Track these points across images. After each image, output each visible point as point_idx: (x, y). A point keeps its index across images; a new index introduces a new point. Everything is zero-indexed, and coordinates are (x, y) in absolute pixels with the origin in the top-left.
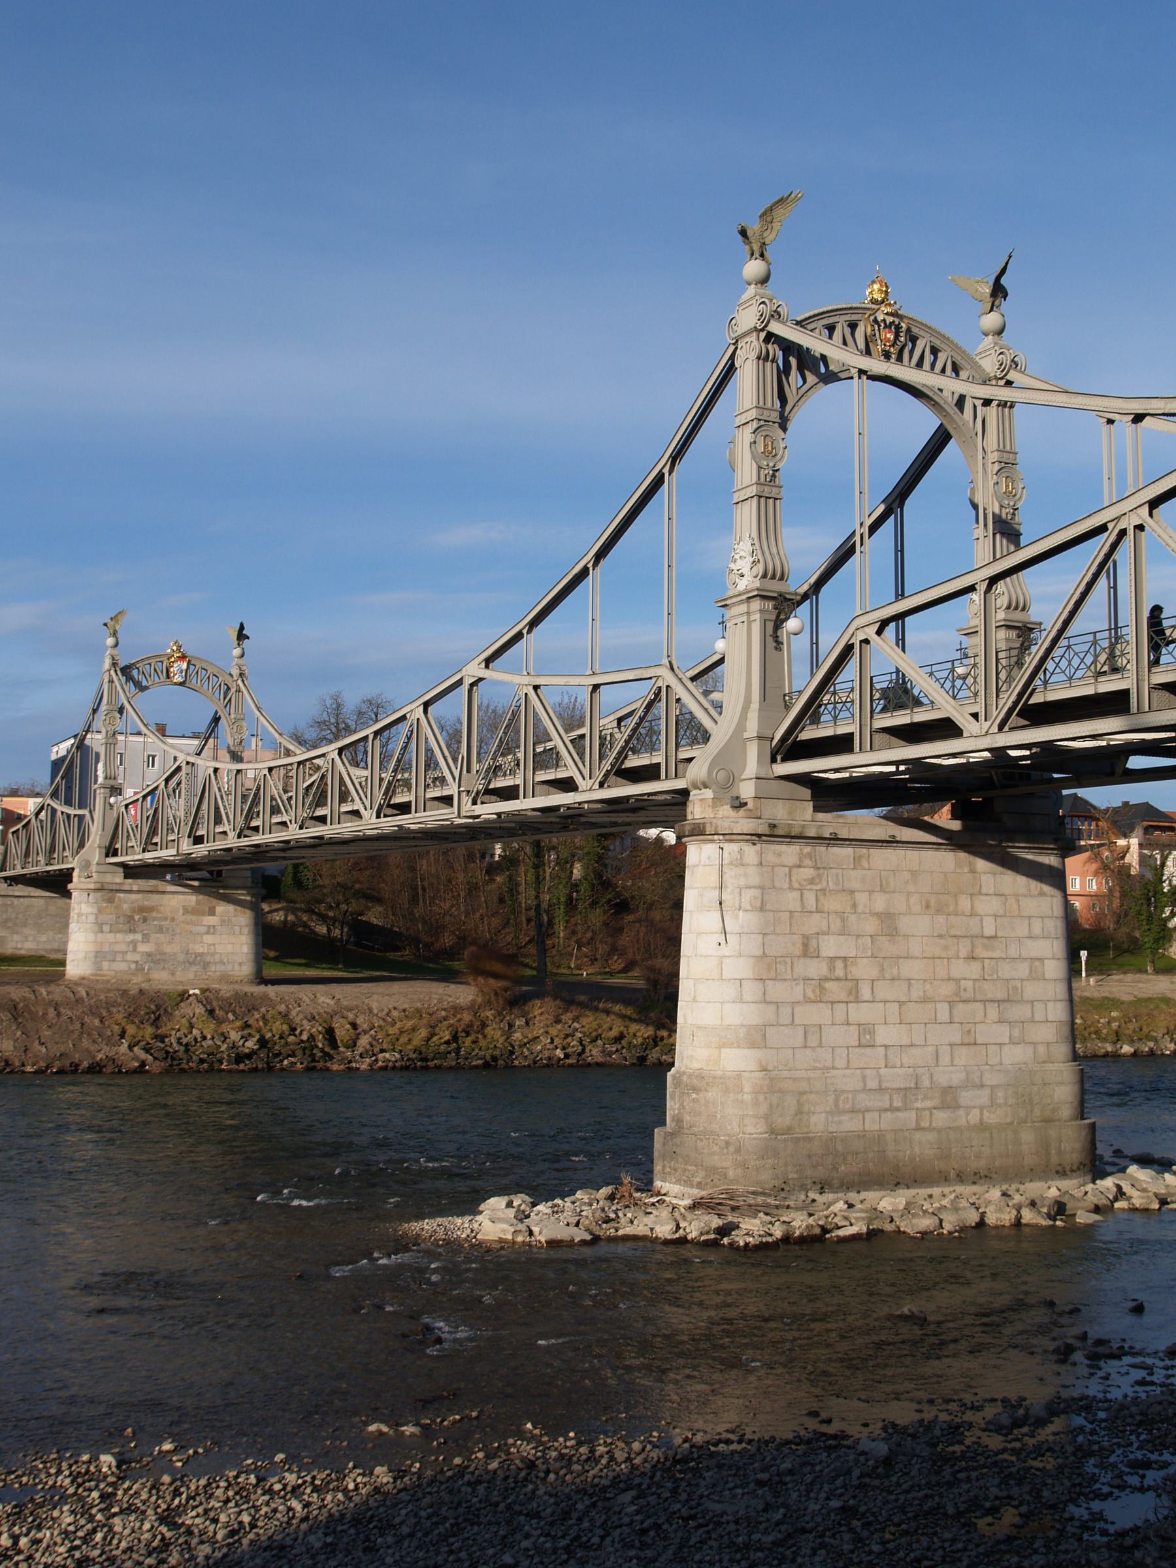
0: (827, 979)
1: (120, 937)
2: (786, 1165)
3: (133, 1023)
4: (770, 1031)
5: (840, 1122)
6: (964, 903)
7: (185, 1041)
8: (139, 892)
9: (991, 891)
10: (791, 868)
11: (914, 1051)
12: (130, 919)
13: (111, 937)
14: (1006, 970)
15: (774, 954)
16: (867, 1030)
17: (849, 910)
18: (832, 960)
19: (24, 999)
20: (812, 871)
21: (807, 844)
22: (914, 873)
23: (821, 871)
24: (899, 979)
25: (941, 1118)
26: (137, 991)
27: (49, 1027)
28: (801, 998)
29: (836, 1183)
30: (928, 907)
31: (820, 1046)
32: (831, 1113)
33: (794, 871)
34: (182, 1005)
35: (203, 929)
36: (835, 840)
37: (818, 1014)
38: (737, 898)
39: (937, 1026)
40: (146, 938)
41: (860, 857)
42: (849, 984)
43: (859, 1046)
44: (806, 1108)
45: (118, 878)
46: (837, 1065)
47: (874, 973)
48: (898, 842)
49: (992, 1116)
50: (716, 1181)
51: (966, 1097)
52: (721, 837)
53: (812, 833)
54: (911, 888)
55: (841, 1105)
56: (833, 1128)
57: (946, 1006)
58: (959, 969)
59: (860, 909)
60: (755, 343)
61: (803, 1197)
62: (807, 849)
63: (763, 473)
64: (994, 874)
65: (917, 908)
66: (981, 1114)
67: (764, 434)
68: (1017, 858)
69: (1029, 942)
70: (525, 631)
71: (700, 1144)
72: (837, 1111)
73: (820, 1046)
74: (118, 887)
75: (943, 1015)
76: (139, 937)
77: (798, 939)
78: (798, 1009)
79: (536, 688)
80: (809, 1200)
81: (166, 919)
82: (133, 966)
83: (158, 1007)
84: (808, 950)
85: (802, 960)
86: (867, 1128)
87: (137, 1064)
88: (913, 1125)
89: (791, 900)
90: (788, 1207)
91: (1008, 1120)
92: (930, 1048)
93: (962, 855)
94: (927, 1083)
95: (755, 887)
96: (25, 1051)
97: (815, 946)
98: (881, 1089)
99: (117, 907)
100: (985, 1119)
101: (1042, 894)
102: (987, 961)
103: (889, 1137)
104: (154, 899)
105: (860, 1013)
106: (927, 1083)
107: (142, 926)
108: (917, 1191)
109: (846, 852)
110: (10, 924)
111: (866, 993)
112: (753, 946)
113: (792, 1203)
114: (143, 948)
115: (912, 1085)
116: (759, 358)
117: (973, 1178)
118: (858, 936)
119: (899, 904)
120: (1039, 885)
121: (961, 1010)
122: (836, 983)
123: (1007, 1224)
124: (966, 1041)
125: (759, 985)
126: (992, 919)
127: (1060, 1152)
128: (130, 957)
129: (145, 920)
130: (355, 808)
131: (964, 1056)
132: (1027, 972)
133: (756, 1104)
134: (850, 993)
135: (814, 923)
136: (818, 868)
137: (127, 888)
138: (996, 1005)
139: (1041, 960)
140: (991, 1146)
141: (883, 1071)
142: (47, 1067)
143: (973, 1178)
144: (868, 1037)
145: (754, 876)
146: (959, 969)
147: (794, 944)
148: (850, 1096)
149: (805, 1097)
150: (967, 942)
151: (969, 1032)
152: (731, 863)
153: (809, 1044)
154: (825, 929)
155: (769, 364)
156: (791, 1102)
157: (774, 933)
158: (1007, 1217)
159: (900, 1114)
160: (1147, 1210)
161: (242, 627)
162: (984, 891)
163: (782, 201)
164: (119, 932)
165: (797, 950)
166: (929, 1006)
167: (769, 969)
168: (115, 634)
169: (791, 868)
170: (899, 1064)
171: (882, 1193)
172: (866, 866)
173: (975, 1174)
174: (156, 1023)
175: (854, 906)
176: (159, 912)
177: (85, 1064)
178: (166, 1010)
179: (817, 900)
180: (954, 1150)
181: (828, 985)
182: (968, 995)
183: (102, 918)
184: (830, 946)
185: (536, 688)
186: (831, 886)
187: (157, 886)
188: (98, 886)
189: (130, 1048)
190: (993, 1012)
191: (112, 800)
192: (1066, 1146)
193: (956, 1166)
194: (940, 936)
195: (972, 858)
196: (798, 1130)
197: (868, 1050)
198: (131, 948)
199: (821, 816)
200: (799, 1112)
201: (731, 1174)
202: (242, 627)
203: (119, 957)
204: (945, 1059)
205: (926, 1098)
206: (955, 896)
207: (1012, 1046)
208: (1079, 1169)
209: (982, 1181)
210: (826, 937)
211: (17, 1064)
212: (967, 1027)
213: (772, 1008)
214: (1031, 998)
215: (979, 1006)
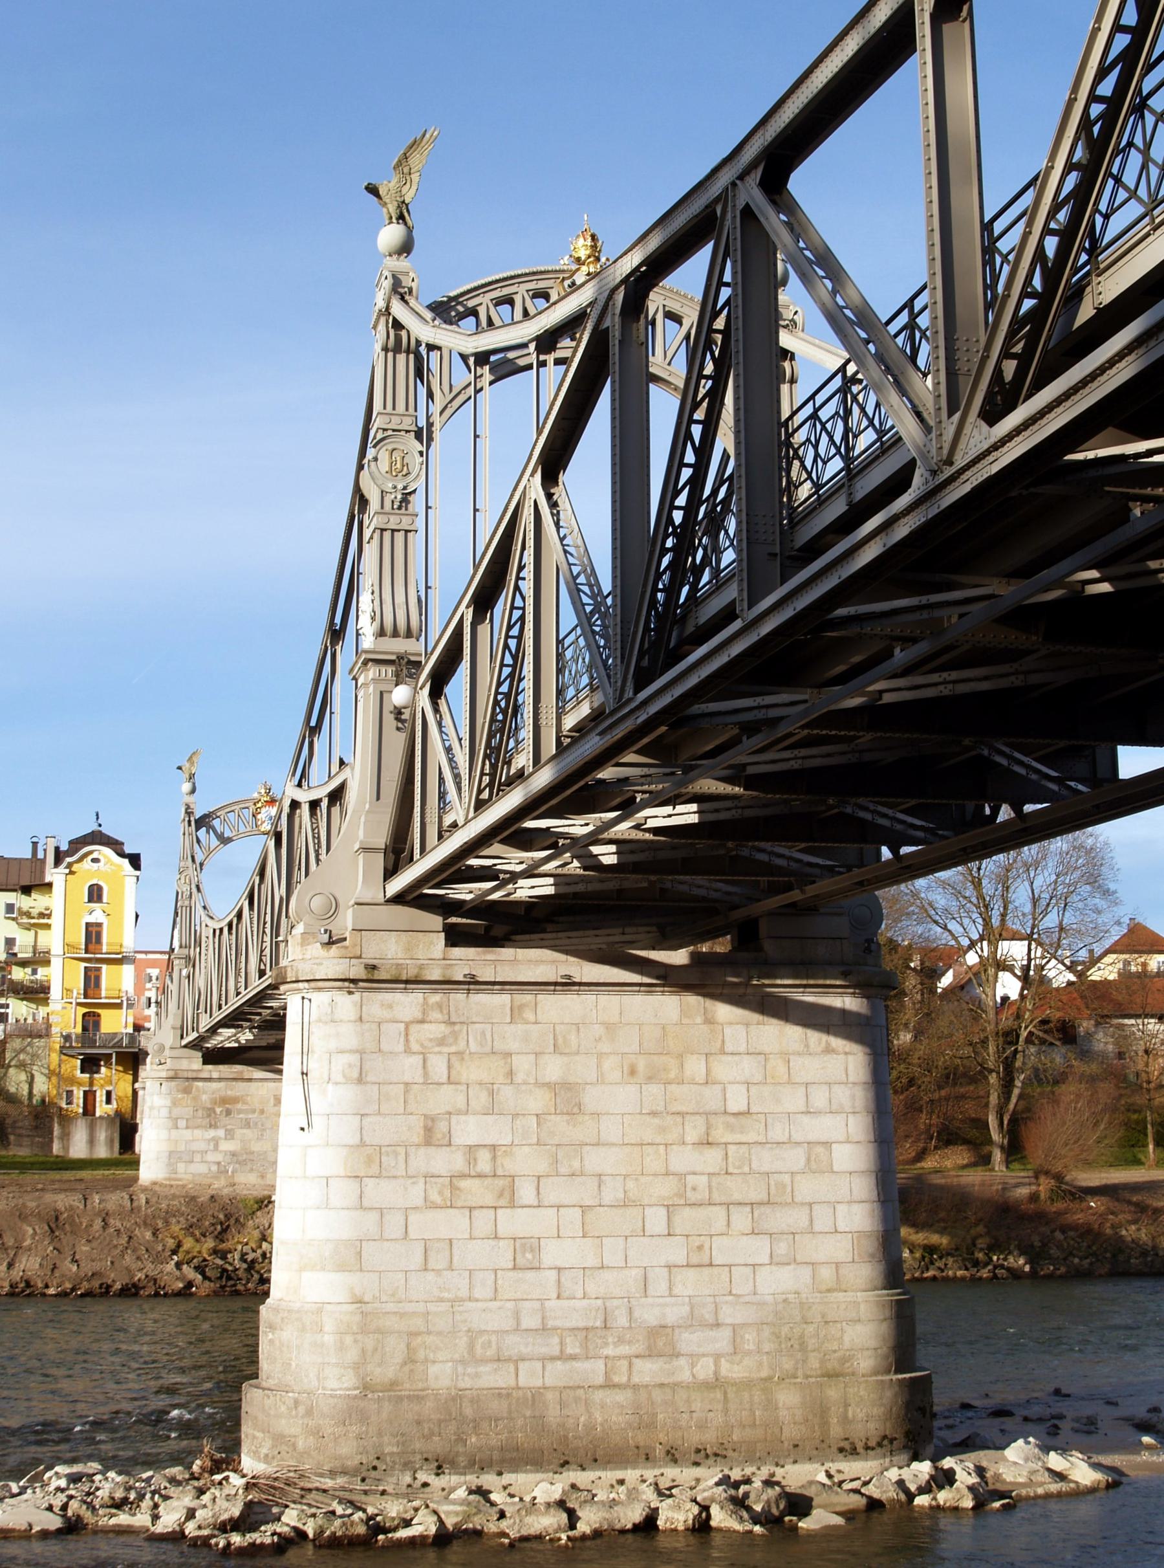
0: (463, 1176)
1: (198, 1133)
2: (380, 1434)
3: (193, 1235)
5: (477, 1375)
6: (695, 1067)
7: (250, 1257)
8: (220, 1079)
9: (742, 1049)
10: (407, 1025)
11: (606, 1275)
12: (210, 1112)
13: (187, 1134)
14: (764, 1160)
15: (376, 1141)
17: (501, 1079)
18: (471, 1149)
19: (71, 1208)
20: (443, 1027)
21: (435, 991)
22: (610, 1027)
23: (457, 1027)
25: (647, 1371)
26: (208, 1197)
27: (89, 1241)
28: (419, 1202)
29: (462, 1461)
30: (633, 1072)
31: (451, 1268)
32: (462, 1362)
33: (414, 1028)
34: (259, 1213)
36: (472, 983)
37: (452, 1223)
39: (645, 1239)
40: (230, 1135)
41: (521, 1007)
42: (500, 1182)
43: (514, 1268)
44: (421, 1355)
45: (194, 1061)
46: (477, 1294)
47: (542, 1167)
48: (574, 984)
49: (736, 1368)
50: (284, 1453)
51: (689, 1341)
52: (306, 985)
53: (435, 975)
54: (605, 1047)
55: (479, 1351)
56: (465, 1383)
57: (663, 1212)
58: (683, 1159)
59: (519, 1078)
61: (408, 1479)
62: (435, 998)
63: (388, 499)
64: (747, 1025)
65: (616, 1075)
67: (390, 447)
68: (786, 1001)
69: (806, 1119)
71: (267, 1402)
72: (472, 1358)
73: (451, 1268)
74: (194, 1075)
76: (221, 1133)
77: (417, 1123)
80: (418, 1484)
81: (254, 1111)
82: (214, 1168)
83: (228, 1217)
84: (430, 1136)
85: (422, 1150)
86: (521, 1384)
87: (181, 1285)
88: (600, 1380)
89: (410, 1068)
90: (383, 1493)
91: (764, 1374)
92: (634, 1272)
93: (692, 1000)
94: (622, 1321)
95: (351, 1051)
96: (53, 1270)
97: (446, 1130)
99: (195, 1099)
100: (724, 1372)
101: (829, 1050)
102: (732, 1148)
103: (550, 1396)
104: (240, 1088)
105: (512, 1222)
106: (622, 1321)
107: (225, 1120)
108: (598, 1473)
109: (502, 1000)
111: (526, 1193)
112: (347, 1131)
113: (389, 1489)
114: (226, 1146)
115: (598, 1324)
116: (386, 349)
117: (694, 1457)
118: (515, 1116)
119: (583, 1069)
120: (824, 1037)
121: (686, 1218)
122: (477, 1181)
123: (681, 1527)
124: (695, 1260)
125: (354, 1185)
126: (743, 1089)
127: (845, 1420)
128: (210, 1157)
129: (228, 1113)
131: (689, 1283)
132: (803, 1162)
133: (341, 1348)
134: (501, 1195)
135: (443, 1099)
136: (454, 1023)
138: (748, 1209)
139: (827, 1145)
140: (726, 1411)
141: (553, 1304)
142: (73, 1289)
143: (694, 1457)
144: (529, 1256)
145: (349, 1036)
146: (683, 1159)
147: (410, 1128)
148: (494, 1338)
149: (419, 1339)
150: (700, 1121)
151: (700, 1248)
152: (319, 1021)
153: (430, 1266)
154: (463, 1106)
155: (401, 358)
156: (396, 1349)
158: (682, 1518)
159: (577, 1365)
160: (956, 1509)
162: (729, 1047)
163: (414, 144)
164: (197, 1127)
165: (417, 1136)
166: (635, 1212)
167: (369, 1160)
168: (191, 777)
169: (407, 1025)
170: (580, 1294)
171: (540, 1476)
172: (532, 1018)
173: (698, 1451)
174: (221, 1237)
175: (511, 1073)
176: (245, 1103)
177: (118, 1286)
178: (237, 1220)
179: (449, 1068)
180: (660, 1416)
181: (464, 1184)
182: (702, 1195)
183: (177, 1112)
184: (469, 1130)
186: (473, 1047)
187: (242, 1072)
188: (171, 1074)
189: (178, 1265)
190: (741, 1219)
192: (858, 1412)
193: (662, 1437)
194: (653, 1114)
195: (709, 1003)
196: (407, 1386)
197: (530, 1275)
198: (212, 1147)
199: (457, 952)
200: (410, 1359)
201: (301, 1444)
203: (198, 1158)
204: (659, 1286)
205: (620, 1341)
206: (680, 1056)
207: (774, 1268)
208: (880, 1445)
209: (711, 1461)
210: (463, 1118)
211: (40, 1285)
212: (697, 1241)
214: (808, 1199)
215: (720, 1212)
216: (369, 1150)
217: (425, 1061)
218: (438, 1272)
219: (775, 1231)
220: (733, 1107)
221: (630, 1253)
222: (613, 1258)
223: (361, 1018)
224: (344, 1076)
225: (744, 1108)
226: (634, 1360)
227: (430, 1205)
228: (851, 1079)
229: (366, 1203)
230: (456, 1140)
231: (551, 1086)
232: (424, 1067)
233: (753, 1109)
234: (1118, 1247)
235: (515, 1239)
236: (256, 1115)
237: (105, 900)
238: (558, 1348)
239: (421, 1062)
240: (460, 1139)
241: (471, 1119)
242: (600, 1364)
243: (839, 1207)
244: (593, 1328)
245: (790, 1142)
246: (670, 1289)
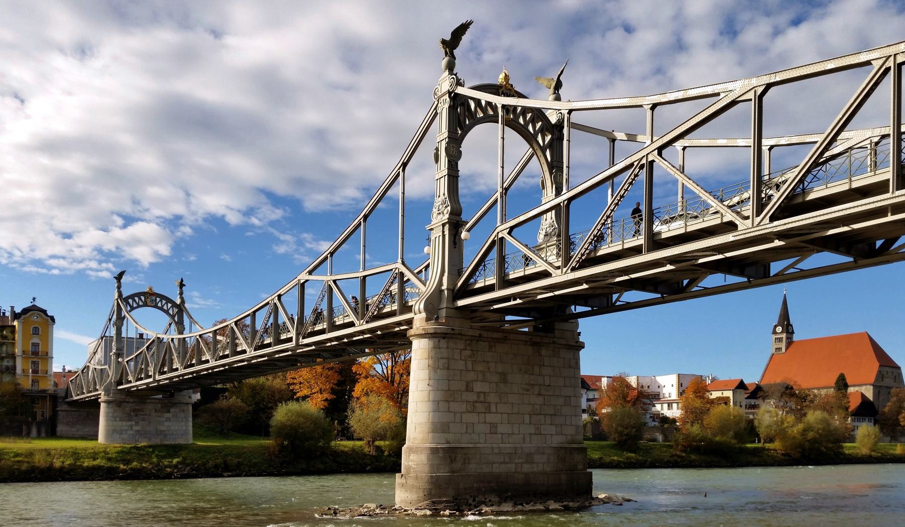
1: (124, 423)
4: (451, 425)
10: (461, 350)
12: (129, 415)
13: (120, 423)
16: (494, 426)
20: (470, 352)
23: (474, 352)
24: (508, 403)
25: (526, 468)
28: (465, 410)
30: (521, 370)
31: (473, 432)
33: (463, 351)
37: (472, 418)
38: (437, 363)
40: (137, 424)
42: (487, 404)
51: (537, 458)
57: (528, 416)
59: (491, 370)
70: (329, 256)
73: (473, 432)
75: (527, 420)
76: (133, 423)
78: (464, 415)
79: (334, 281)
85: (465, 393)
105: (490, 418)
110: (70, 424)
111: (493, 409)
115: (514, 452)
118: (490, 383)
124: (537, 432)
130: (243, 349)
136: (474, 351)
137: (127, 400)
138: (550, 416)
151: (538, 428)
153: (468, 432)
157: (453, 380)
159: (508, 465)
161: (182, 280)
164: (124, 420)
165: (464, 388)
169: (461, 350)
170: (508, 442)
175: (489, 368)
181: (477, 405)
185: (334, 281)
191: (120, 360)
197: (494, 435)
202: (182, 280)
203: (124, 432)
213: (452, 414)
216: (451, 392)
219: (504, 433)
220: (546, 384)
221: (520, 429)
222: (516, 431)
223: (448, 348)
224: (443, 367)
226: (523, 464)
230: (475, 390)
231: (500, 373)
232: (466, 364)
233: (551, 385)
234: (172, 513)
235: (490, 423)
236: (148, 416)
237: (40, 334)
238: (503, 460)
242: (514, 465)
243: (573, 417)
244: (512, 453)
246: (530, 441)
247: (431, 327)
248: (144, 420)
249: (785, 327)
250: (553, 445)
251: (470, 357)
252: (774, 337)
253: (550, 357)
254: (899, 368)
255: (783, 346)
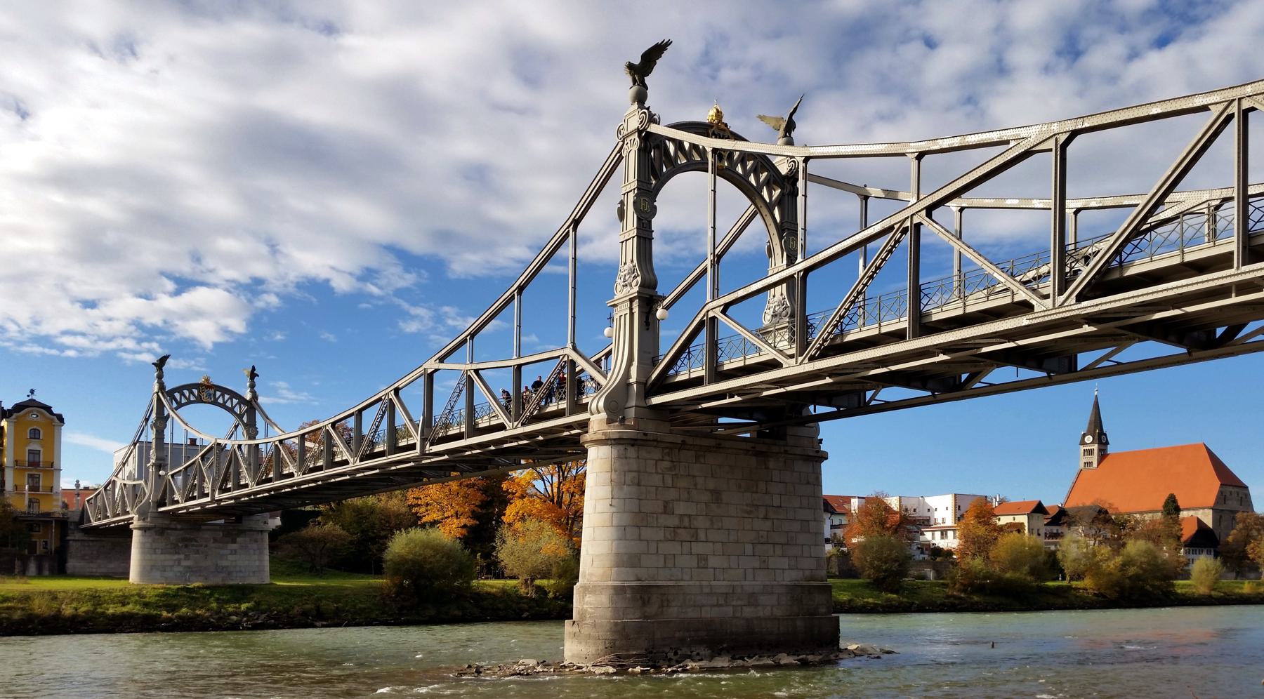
0: (678, 528)
1: (168, 557)
10: (657, 461)
13: (162, 557)
16: (702, 558)
23: (675, 464)
25: (748, 612)
28: (663, 539)
31: (674, 567)
33: (659, 463)
35: (229, 552)
37: (674, 548)
40: (187, 557)
42: (693, 530)
51: (763, 599)
59: (699, 487)
60: (637, 139)
66: (772, 609)
73: (674, 567)
76: (182, 556)
77: (661, 504)
78: (661, 545)
79: (476, 371)
85: (663, 515)
98: (711, 593)
102: (775, 520)
105: (698, 548)
111: (702, 536)
122: (683, 530)
134: (693, 536)
137: (173, 526)
144: (703, 562)
151: (764, 561)
161: (254, 369)
165: (661, 509)
169: (657, 461)
175: (695, 485)
181: (679, 531)
185: (476, 371)
186: (682, 473)
190: (779, 551)
191: (162, 473)
198: (177, 564)
202: (254, 369)
210: (678, 502)
215: (771, 546)
217: (663, 477)
218: (670, 568)
224: (632, 482)
225: (779, 505)
227: (667, 540)
228: (614, 524)
229: (642, 538)
239: (662, 478)
240: (677, 512)
241: (681, 503)
245: (795, 520)
247: (615, 431)
248: (197, 552)
249: (1096, 437)
250: (784, 583)
251: (670, 469)
252: (1082, 448)
253: (780, 470)
254: (1246, 488)
255: (1094, 459)
